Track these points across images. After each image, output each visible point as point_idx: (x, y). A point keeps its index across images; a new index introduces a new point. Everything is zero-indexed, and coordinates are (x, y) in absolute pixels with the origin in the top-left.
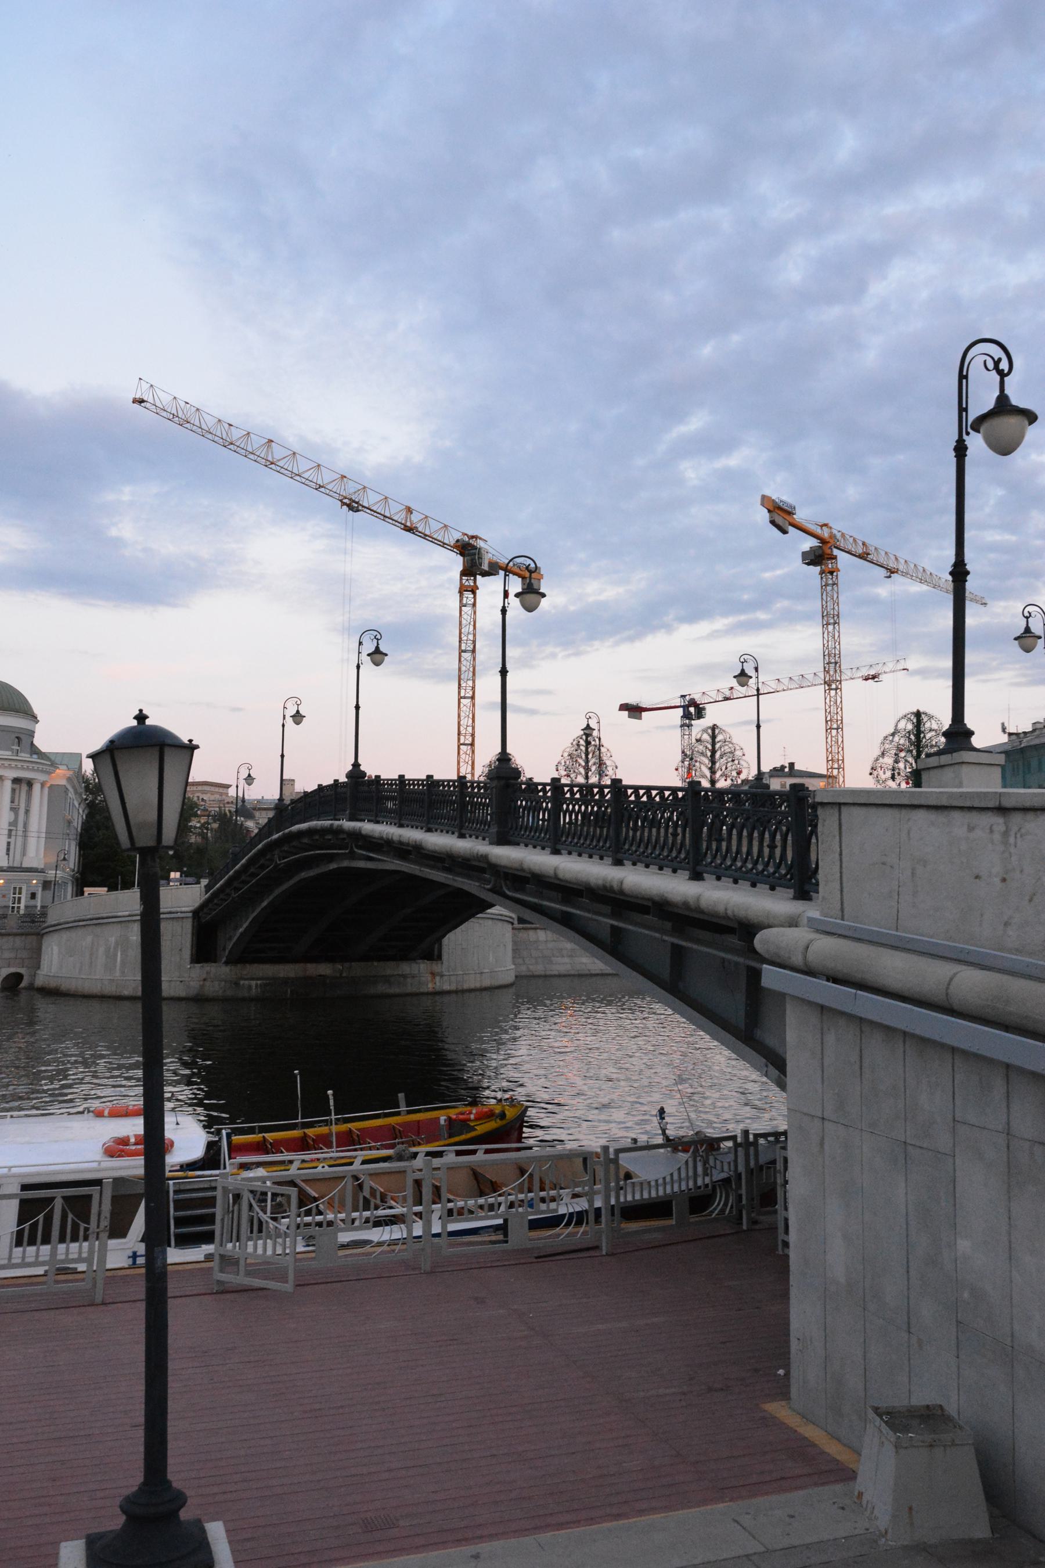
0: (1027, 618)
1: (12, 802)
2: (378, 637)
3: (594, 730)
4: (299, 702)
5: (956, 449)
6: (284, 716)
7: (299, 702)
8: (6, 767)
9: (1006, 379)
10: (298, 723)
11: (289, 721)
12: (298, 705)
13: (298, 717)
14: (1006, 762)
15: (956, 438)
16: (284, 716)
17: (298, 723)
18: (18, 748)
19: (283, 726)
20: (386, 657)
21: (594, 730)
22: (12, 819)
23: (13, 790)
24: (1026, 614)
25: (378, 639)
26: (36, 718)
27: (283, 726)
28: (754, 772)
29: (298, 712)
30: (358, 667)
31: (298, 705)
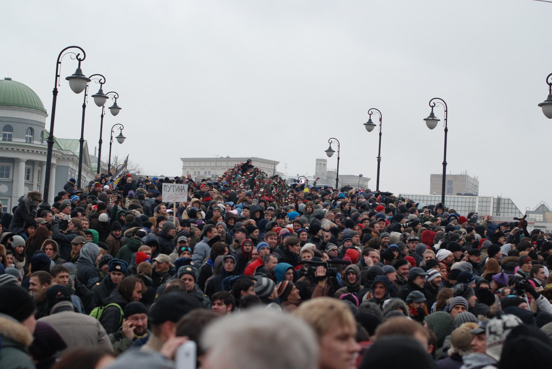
0: (432, 107)
1: (28, 178)
2: (116, 96)
3: (334, 152)
4: (122, 128)
5: (53, 92)
6: (112, 137)
7: (122, 128)
8: (15, 151)
9: (81, 62)
10: (121, 142)
11: (115, 140)
12: (121, 129)
13: (121, 138)
14: (431, 193)
15: (54, 87)
16: (112, 137)
17: (121, 142)
18: (31, 136)
19: (111, 144)
20: (120, 110)
21: (334, 152)
22: (170, 179)
23: (28, 171)
24: (432, 104)
25: (116, 98)
26: (46, 113)
27: (111, 144)
28: (70, 203)
29: (121, 134)
30: (102, 116)
31: (121, 129)
